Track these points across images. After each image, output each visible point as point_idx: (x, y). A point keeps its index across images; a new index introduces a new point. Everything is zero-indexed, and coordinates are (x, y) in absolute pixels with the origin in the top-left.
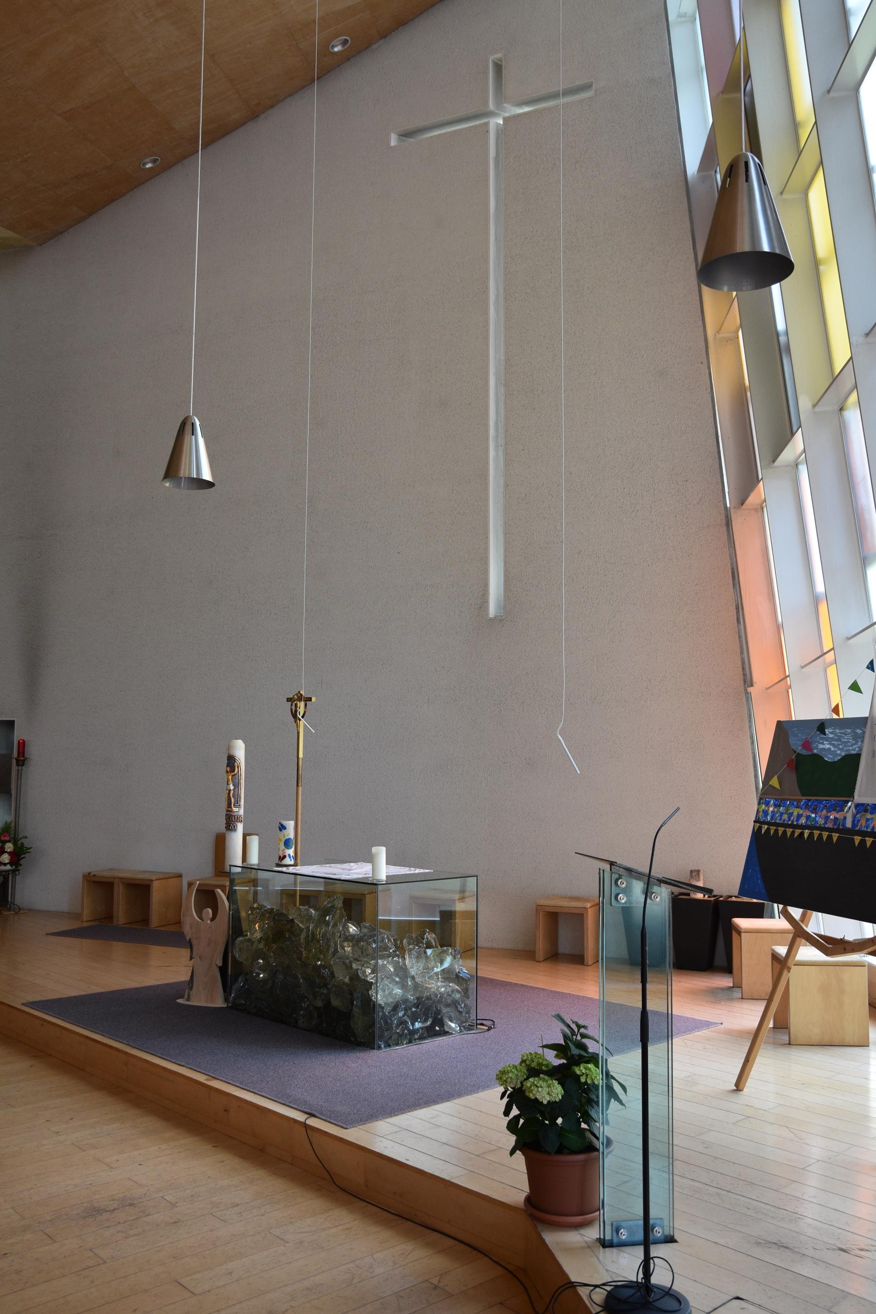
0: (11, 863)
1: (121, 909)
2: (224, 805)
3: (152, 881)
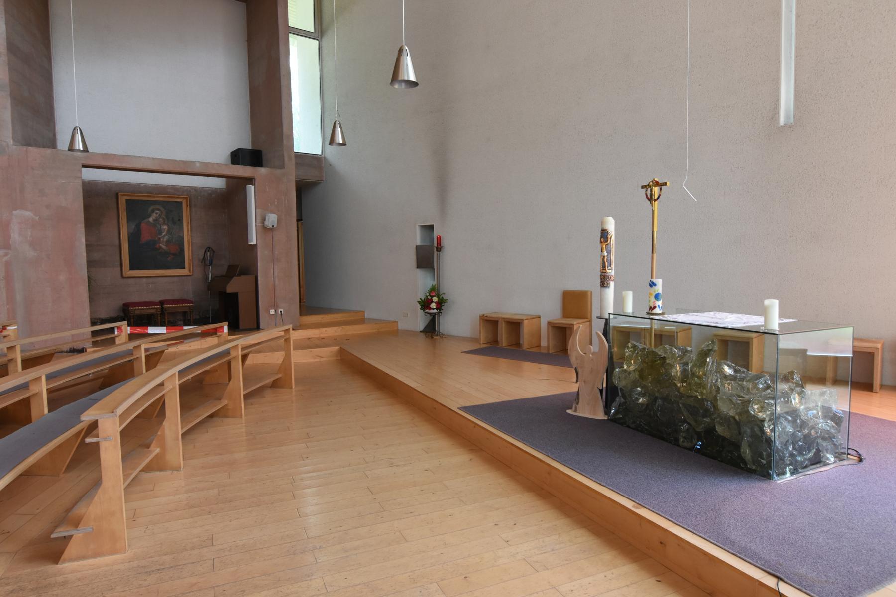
0: (437, 309)
1: (503, 339)
2: (599, 267)
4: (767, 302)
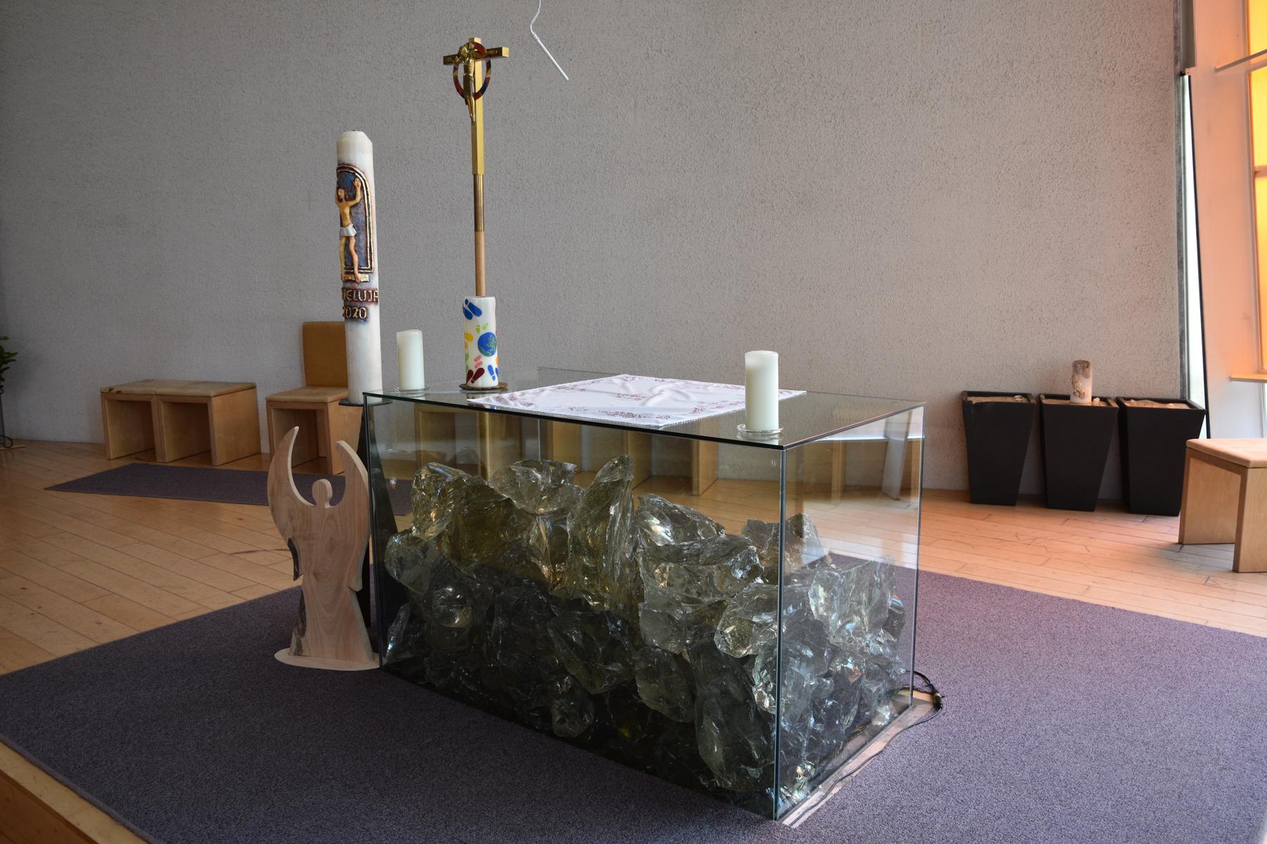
2: (339, 267)
3: (209, 397)
4: (752, 359)
